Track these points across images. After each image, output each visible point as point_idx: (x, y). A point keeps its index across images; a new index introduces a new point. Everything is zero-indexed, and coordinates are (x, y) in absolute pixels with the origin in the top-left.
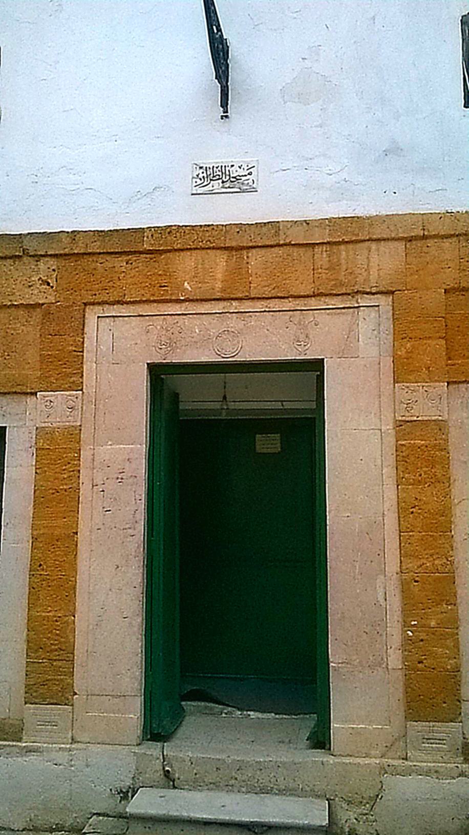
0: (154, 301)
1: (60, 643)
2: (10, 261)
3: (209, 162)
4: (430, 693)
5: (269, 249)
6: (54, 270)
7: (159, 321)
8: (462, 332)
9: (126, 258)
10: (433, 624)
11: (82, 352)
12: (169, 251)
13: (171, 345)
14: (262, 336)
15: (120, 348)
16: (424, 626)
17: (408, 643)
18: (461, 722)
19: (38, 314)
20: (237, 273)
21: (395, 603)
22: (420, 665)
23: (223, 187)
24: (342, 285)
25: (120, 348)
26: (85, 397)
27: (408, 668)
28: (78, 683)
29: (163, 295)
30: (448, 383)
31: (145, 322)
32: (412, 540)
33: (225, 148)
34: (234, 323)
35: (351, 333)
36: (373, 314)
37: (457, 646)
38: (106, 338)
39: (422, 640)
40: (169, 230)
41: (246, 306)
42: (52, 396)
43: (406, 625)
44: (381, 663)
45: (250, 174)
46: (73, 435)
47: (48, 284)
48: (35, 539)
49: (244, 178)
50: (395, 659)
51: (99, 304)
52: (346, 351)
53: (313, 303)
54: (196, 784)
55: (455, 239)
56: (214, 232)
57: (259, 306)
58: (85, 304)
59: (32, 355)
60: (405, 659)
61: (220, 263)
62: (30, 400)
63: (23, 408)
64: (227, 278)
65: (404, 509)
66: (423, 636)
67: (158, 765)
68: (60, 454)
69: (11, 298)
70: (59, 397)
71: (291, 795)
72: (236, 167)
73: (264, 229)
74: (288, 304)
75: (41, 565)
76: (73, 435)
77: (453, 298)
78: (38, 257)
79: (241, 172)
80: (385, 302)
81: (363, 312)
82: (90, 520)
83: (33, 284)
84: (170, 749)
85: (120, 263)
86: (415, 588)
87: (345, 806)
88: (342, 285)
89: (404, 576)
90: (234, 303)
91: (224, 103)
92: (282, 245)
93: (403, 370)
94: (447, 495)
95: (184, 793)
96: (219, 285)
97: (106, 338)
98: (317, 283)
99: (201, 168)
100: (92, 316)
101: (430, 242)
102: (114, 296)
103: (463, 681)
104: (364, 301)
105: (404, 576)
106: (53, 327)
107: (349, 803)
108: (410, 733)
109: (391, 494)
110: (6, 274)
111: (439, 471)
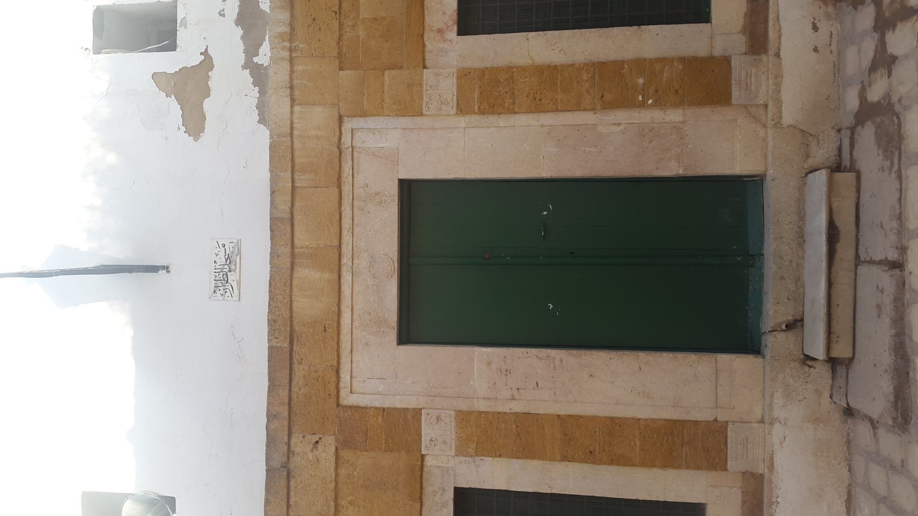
2: (292, 483)
9: (296, 366)
10: (641, 81)
12: (292, 322)
14: (376, 237)
17: (659, 104)
21: (622, 116)
22: (680, 92)
23: (235, 271)
30: (425, 67)
33: (194, 271)
36: (358, 135)
39: (656, 91)
40: (272, 323)
41: (346, 250)
45: (224, 246)
46: (464, 418)
47: (317, 442)
48: (565, 458)
49: (228, 252)
50: (674, 116)
51: (338, 392)
61: (301, 273)
65: (537, 106)
66: (652, 91)
76: (464, 418)
78: (290, 453)
79: (222, 254)
80: (348, 125)
82: (545, 403)
86: (608, 97)
91: (154, 269)
96: (327, 276)
100: (348, 399)
104: (346, 140)
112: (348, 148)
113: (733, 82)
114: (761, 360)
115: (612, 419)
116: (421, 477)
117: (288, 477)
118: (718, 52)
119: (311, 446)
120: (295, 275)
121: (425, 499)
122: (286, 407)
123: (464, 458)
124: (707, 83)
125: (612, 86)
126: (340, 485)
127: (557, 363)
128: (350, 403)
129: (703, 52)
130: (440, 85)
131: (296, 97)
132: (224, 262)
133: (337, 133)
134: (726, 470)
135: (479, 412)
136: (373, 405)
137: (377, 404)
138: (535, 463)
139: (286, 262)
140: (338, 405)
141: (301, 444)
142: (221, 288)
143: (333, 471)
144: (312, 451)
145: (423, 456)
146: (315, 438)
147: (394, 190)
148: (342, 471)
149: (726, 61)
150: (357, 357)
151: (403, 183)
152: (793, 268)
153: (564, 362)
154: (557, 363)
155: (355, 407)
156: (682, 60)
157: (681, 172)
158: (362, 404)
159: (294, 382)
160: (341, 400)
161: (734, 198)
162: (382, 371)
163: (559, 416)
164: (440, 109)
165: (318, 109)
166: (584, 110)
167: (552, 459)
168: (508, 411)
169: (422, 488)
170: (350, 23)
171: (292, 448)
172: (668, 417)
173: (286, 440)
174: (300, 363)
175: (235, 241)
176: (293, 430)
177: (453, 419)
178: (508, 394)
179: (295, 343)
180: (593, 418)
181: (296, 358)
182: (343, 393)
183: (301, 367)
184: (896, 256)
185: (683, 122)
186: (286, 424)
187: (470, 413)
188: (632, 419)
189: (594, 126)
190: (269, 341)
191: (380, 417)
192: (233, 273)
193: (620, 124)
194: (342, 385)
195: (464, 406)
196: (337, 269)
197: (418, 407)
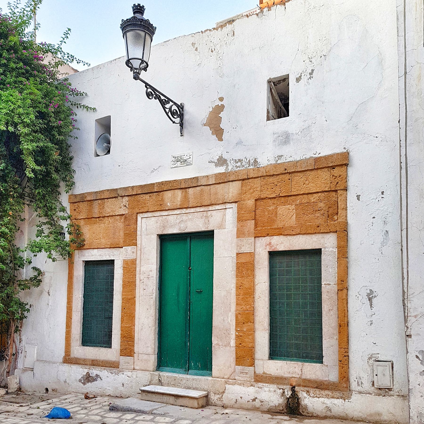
0: (158, 211)
2: (114, 199)
5: (195, 188)
7: (161, 218)
9: (149, 195)
10: (245, 330)
11: (136, 231)
12: (162, 191)
13: (164, 227)
15: (149, 228)
16: (242, 331)
17: (237, 337)
20: (186, 198)
22: (241, 345)
23: (181, 164)
27: (236, 346)
28: (136, 350)
29: (161, 208)
30: (255, 237)
32: (240, 299)
34: (185, 217)
35: (223, 219)
36: (231, 210)
38: (144, 226)
39: (241, 336)
40: (162, 183)
41: (188, 211)
43: (237, 331)
46: (133, 262)
48: (123, 299)
50: (233, 343)
52: (221, 226)
53: (211, 208)
54: (168, 385)
55: (260, 178)
57: (192, 210)
58: (137, 213)
61: (179, 193)
62: (121, 249)
63: (119, 252)
65: (239, 287)
66: (241, 334)
67: (157, 378)
70: (129, 248)
71: (197, 390)
72: (185, 156)
74: (202, 209)
76: (133, 262)
78: (122, 197)
80: (234, 206)
82: (139, 292)
84: (161, 374)
85: (147, 197)
87: (213, 394)
90: (185, 210)
92: (199, 186)
93: (240, 234)
95: (164, 387)
96: (179, 203)
100: (139, 217)
101: (250, 180)
104: (228, 206)
107: (215, 394)
109: (234, 281)
113: (244, 367)
114: (151, 369)
115: (134, 316)
117: (115, 197)
118: (256, 362)
121: (111, 249)
124: (245, 355)
125: (245, 318)
126: (114, 217)
127: (151, 297)
128: (138, 218)
131: (245, 181)
133: (231, 201)
135: (136, 268)
140: (137, 213)
143: (118, 214)
147: (209, 229)
148: (118, 217)
149: (252, 364)
150: (153, 219)
151: (213, 231)
152: (188, 384)
154: (151, 297)
159: (144, 195)
161: (205, 365)
162: (149, 228)
163: (135, 297)
165: (24, 277)
167: (122, 295)
169: (114, 248)
170: (275, 202)
171: (125, 197)
172: (135, 336)
176: (130, 197)
178: (141, 278)
180: (134, 310)
183: (149, 197)
186: (131, 194)
187: (135, 264)
195: (138, 262)
196: (181, 207)
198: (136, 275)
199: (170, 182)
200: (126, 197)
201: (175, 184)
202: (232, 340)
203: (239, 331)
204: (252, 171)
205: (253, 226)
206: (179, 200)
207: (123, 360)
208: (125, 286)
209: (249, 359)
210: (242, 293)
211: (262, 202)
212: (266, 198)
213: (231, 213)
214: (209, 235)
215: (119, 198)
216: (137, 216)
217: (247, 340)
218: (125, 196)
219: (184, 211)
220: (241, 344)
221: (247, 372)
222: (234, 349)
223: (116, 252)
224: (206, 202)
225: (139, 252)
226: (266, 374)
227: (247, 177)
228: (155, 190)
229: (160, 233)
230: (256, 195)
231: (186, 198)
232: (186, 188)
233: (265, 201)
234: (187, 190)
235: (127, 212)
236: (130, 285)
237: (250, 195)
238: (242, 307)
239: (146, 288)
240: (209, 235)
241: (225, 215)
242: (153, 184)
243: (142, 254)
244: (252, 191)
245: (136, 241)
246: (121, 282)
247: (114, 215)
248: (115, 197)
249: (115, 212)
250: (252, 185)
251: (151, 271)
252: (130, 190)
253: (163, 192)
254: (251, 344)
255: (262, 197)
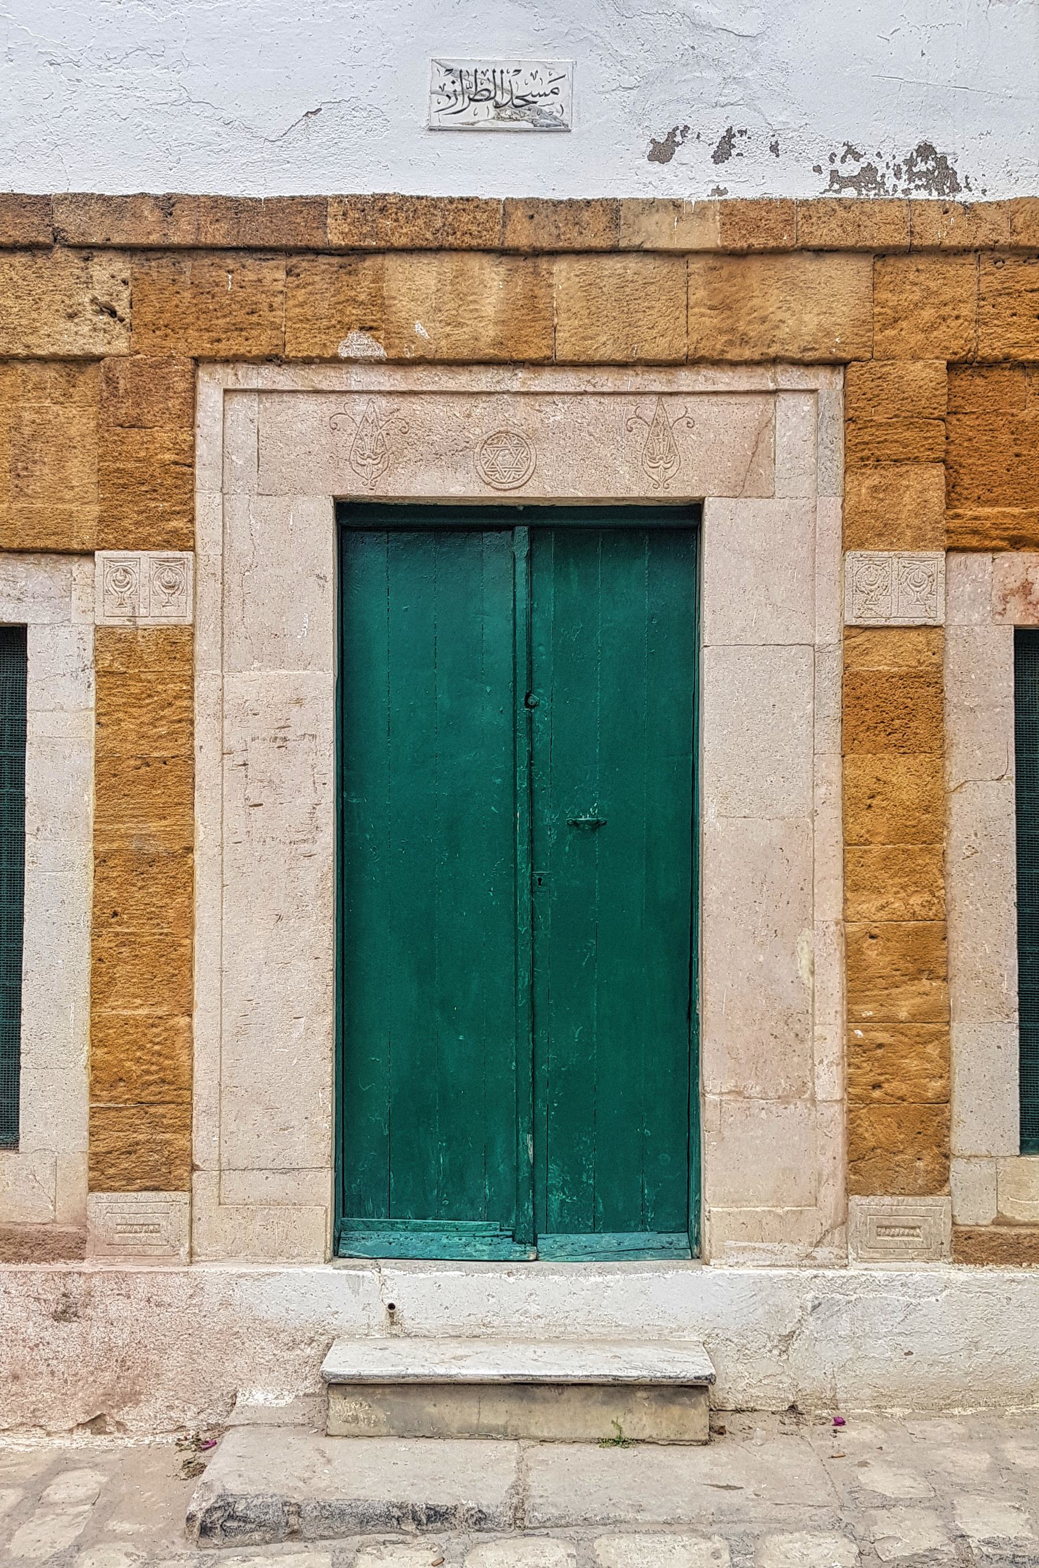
1: (163, 1069)
3: (466, 60)
4: (897, 1138)
6: (125, 282)
8: (977, 450)
9: (283, 262)
13: (460, 274)
14: (577, 451)
18: (949, 1194)
19: (89, 382)
20: (533, 308)
21: (833, 978)
22: (877, 1094)
23: (499, 118)
24: (744, 341)
25: (275, 467)
26: (201, 564)
28: (203, 1142)
31: (326, 407)
32: (868, 860)
34: (520, 412)
36: (806, 404)
37: (946, 1057)
39: (880, 1046)
41: (546, 381)
42: (130, 559)
43: (852, 1019)
44: (801, 1090)
46: (177, 644)
47: (113, 313)
48: (101, 860)
50: (829, 1083)
51: (226, 361)
53: (686, 380)
56: (478, 215)
58: (197, 361)
59: (80, 471)
60: (850, 1082)
61: (491, 280)
62: (79, 568)
64: (503, 317)
66: (882, 1037)
68: (148, 680)
69: (26, 340)
70: (145, 560)
72: (525, 73)
73: (586, 215)
75: (115, 914)
76: (177, 644)
77: (963, 382)
78: (87, 250)
80: (824, 380)
81: (786, 402)
82: (214, 819)
83: (72, 312)
85: (273, 273)
86: (872, 953)
88: (744, 341)
89: (851, 928)
94: (937, 772)
96: (490, 332)
97: (243, 438)
98: (695, 337)
99: (450, 71)
100: (210, 387)
102: (262, 343)
103: (954, 1122)
104: (788, 378)
105: (851, 928)
106: (126, 409)
108: (857, 1216)
110: (16, 286)
111: (869, 1073)
112: (774, 380)
116: (45, 551)
117: (31, 248)
119: (104, 299)
120: (486, 261)
122: (190, 240)
123: (90, 647)
126: (21, 368)
128: (201, 387)
129: (959, 1140)
130: (906, 585)
132: (516, 93)
133: (809, 356)
134: (91, 1189)
135: (192, 677)
136: (199, 440)
137: (201, 449)
138: (89, 798)
139: (521, 235)
140: (197, 361)
141: (108, 273)
142: (457, 87)
144: (94, 301)
145: (89, 554)
146: (122, 308)
150: (307, 405)
153: (307, 861)
155: (194, 398)
156: (945, 1099)
157: (710, 1097)
158: (200, 415)
160: (210, 368)
163: (190, 849)
164: (858, 590)
166: (846, 900)
168: (197, 743)
171: (103, 258)
173: (117, 239)
174: (289, 273)
175: (565, 118)
177: (173, 621)
179: (335, 260)
181: (303, 263)
182: (104, 553)
183: (281, 275)
184: (719, 242)
185: (813, 1100)
187: (190, 660)
188: (191, 1002)
189: (807, 921)
190: (339, 199)
191: (174, 457)
192: (493, 112)
193: (813, 973)
194: (242, 369)
195: (204, 646)
196: (504, 354)
197: (199, 544)
198: (192, 722)
199: (435, 203)
200: (111, 255)
201: (465, 218)
202: (819, 1069)
203: (869, 1020)
204: (934, 214)
205: (936, 497)
206: (489, 311)
207: (115, 1209)
208: (111, 775)
209: (928, 1159)
210: (883, 830)
211: (978, 381)
212: (1006, 358)
213: (803, 421)
214: (672, 530)
215: (60, 254)
216: (194, 375)
217: (912, 1064)
218: (104, 248)
219: (519, 380)
220: (877, 1086)
221: (910, 1221)
222: (835, 1116)
223: (42, 576)
224: (663, 342)
225: (210, 590)
226: (1011, 1224)
227: (906, 242)
228: (335, 239)
229: (358, 487)
230: (957, 338)
231: (533, 308)
232: (537, 253)
233: (995, 375)
234: (544, 264)
235: (121, 346)
236: (149, 770)
237: (921, 336)
238: (883, 901)
239: (265, 797)
240: (672, 530)
241: (767, 424)
242: (319, 204)
243: (234, 600)
244: (928, 314)
245: (192, 521)
246: (84, 760)
247: (21, 351)
248: (31, 248)
249: (32, 340)
250: (932, 285)
251: (299, 702)
252: (151, 215)
253: (379, 259)
254: (937, 1084)
255: (985, 351)
